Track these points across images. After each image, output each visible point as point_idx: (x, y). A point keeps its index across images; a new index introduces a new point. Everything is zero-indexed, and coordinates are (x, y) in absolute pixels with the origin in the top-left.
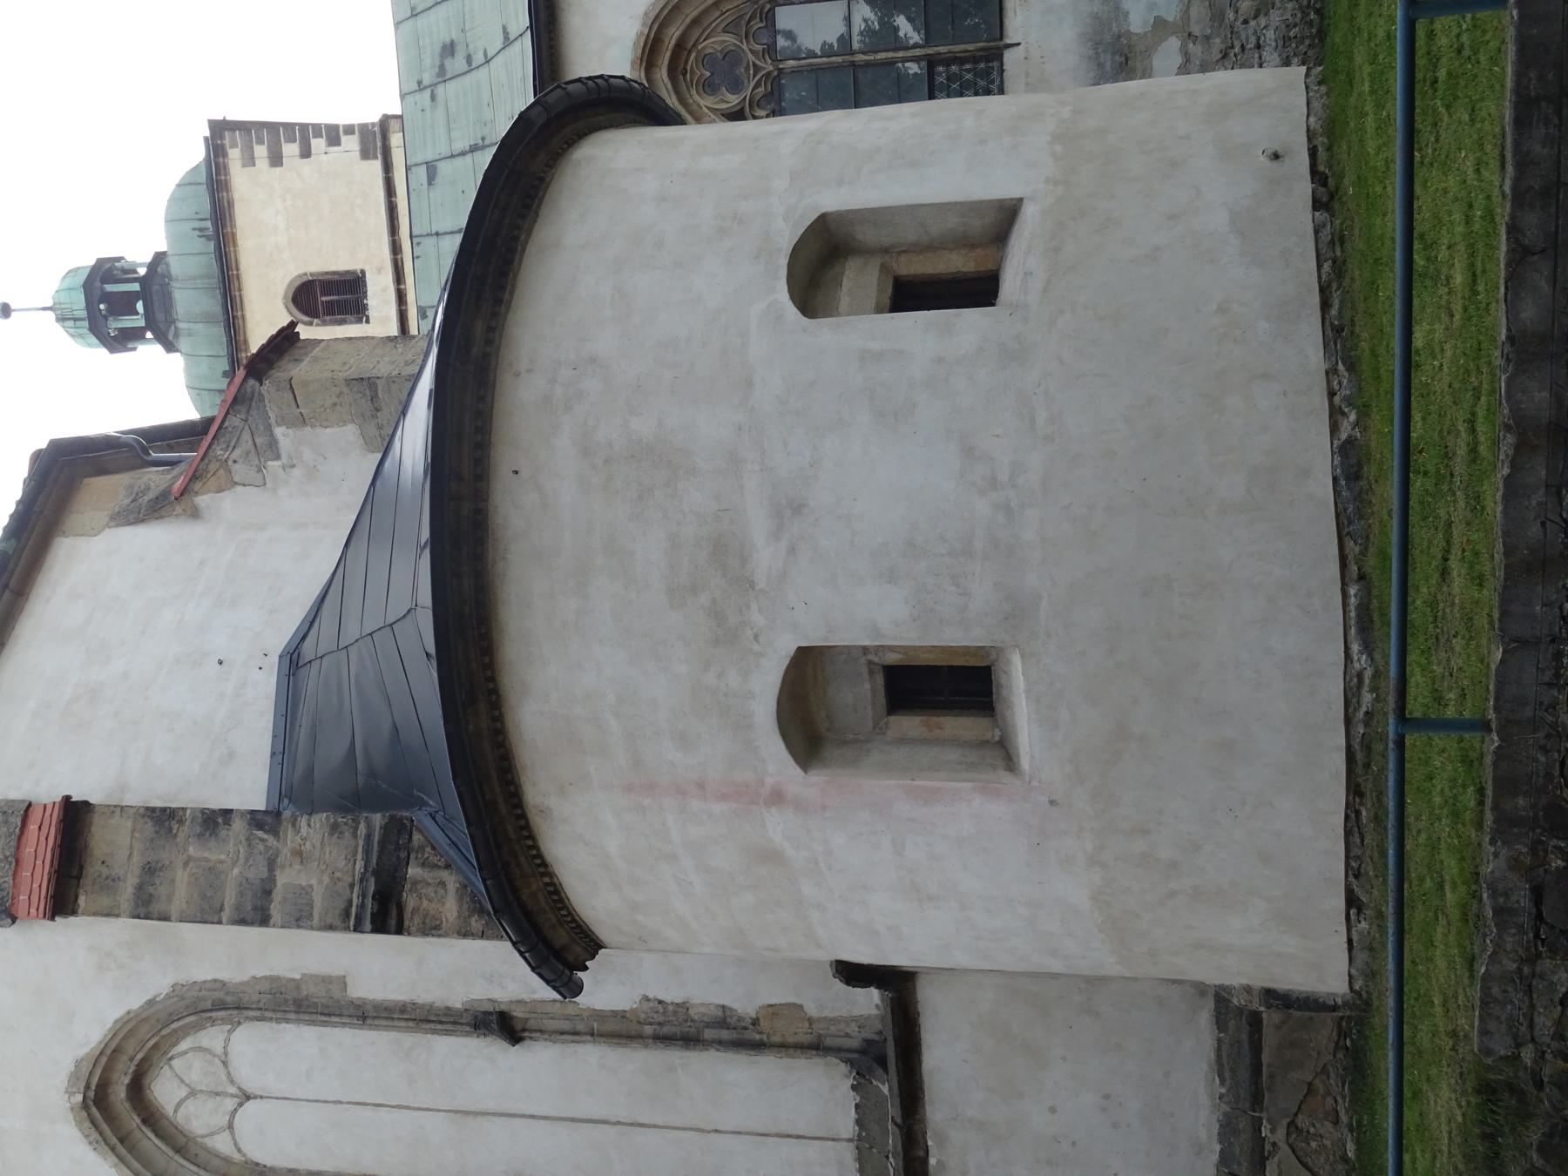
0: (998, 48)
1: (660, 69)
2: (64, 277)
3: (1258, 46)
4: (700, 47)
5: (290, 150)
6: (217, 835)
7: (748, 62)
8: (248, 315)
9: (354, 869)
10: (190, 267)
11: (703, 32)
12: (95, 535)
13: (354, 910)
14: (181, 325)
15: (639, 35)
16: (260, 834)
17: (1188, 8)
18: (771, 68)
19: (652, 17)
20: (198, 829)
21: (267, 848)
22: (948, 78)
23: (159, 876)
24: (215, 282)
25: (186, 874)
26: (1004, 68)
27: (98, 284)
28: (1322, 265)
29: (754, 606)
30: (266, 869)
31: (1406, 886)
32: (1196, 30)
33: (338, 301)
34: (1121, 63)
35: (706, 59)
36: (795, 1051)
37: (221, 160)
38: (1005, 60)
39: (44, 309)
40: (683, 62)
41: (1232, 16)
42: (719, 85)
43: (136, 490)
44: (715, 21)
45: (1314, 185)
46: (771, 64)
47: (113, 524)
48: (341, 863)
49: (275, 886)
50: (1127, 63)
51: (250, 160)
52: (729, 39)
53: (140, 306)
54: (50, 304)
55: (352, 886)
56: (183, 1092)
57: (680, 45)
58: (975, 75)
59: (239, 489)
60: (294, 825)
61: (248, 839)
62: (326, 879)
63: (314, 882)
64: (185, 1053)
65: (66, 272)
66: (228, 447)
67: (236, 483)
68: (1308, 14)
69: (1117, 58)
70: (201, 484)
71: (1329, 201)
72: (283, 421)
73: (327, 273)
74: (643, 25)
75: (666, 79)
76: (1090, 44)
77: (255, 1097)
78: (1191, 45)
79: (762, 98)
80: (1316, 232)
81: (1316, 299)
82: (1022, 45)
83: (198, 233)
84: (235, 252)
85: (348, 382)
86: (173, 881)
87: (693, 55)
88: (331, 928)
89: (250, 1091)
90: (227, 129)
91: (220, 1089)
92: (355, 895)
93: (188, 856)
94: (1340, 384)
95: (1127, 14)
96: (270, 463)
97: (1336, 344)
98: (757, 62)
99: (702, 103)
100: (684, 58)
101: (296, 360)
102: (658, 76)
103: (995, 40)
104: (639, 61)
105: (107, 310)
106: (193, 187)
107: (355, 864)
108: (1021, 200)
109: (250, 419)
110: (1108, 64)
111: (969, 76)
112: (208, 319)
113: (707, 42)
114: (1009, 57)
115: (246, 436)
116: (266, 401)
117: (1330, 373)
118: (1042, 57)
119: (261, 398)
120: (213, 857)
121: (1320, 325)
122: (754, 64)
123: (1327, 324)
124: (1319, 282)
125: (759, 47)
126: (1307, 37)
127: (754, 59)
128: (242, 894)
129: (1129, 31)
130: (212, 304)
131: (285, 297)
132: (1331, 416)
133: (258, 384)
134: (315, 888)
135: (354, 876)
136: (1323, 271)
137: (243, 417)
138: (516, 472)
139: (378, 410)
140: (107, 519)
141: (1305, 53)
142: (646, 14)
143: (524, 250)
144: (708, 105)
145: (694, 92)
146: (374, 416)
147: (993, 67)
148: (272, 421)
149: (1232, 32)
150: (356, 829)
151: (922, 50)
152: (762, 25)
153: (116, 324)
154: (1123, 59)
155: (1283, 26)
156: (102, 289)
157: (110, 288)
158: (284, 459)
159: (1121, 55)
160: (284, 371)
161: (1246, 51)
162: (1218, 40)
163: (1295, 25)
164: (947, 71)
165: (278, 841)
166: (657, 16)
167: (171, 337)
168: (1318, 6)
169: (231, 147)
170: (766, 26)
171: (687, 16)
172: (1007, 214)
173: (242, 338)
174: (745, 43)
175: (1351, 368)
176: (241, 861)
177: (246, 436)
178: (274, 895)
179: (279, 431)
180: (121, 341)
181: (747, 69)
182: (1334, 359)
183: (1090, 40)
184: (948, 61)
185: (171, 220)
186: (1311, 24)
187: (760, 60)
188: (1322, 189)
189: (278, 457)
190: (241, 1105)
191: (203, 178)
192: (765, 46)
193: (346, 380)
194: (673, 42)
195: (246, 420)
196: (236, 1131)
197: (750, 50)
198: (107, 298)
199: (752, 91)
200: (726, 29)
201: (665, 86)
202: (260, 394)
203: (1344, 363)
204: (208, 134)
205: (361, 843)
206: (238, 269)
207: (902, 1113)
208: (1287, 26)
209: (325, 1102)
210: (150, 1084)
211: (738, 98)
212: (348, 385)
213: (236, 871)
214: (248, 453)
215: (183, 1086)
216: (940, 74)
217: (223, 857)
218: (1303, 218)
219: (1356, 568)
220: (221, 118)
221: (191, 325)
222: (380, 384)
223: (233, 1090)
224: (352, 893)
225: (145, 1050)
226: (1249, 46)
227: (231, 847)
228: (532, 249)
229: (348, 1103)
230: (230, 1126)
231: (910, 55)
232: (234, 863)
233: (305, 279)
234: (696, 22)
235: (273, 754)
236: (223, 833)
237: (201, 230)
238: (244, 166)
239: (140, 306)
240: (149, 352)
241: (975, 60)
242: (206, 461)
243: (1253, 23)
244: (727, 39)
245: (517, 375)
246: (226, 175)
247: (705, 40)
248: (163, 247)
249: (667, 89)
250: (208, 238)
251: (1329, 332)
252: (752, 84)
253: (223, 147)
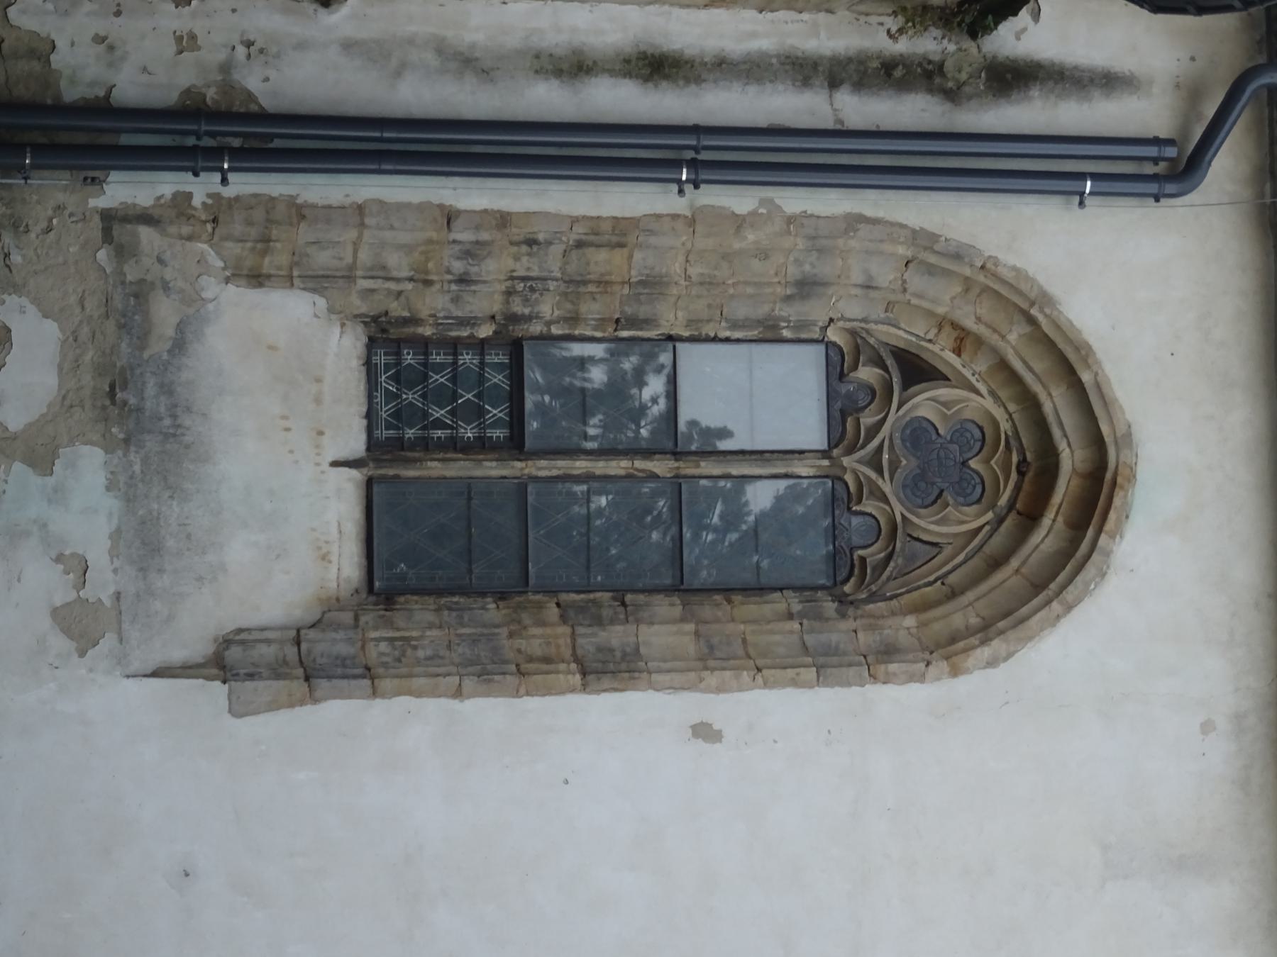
0: (379, 462)
1: (1074, 469)
4: (990, 515)
15: (1117, 533)
18: (846, 461)
22: (481, 412)
26: (365, 422)
34: (124, 387)
35: (980, 494)
36: (707, 334)
40: (1026, 486)
42: (951, 441)
44: (960, 565)
46: (844, 469)
50: (112, 387)
52: (928, 525)
57: (1031, 518)
58: (426, 415)
74: (1108, 554)
75: (1062, 446)
79: (866, 407)
82: (331, 459)
87: (1003, 501)
98: (873, 475)
99: (988, 403)
100: (1022, 495)
102: (1080, 454)
103: (383, 479)
104: (1119, 480)
110: (151, 389)
111: (438, 413)
114: (356, 444)
118: (288, 430)
122: (880, 471)
127: (880, 482)
129: (106, 453)
144: (979, 399)
145: (1005, 426)
151: (535, 472)
152: (861, 552)
159: (125, 403)
164: (482, 427)
170: (852, 550)
171: (1017, 571)
174: (899, 518)
181: (894, 466)
183: (187, 447)
184: (482, 446)
187: (868, 478)
194: (1046, 521)
197: (887, 501)
199: (884, 419)
200: (935, 550)
207: (493, 696)
211: (915, 407)
216: (499, 367)
234: (996, 563)
241: (426, 446)
244: (933, 527)
247: (983, 526)
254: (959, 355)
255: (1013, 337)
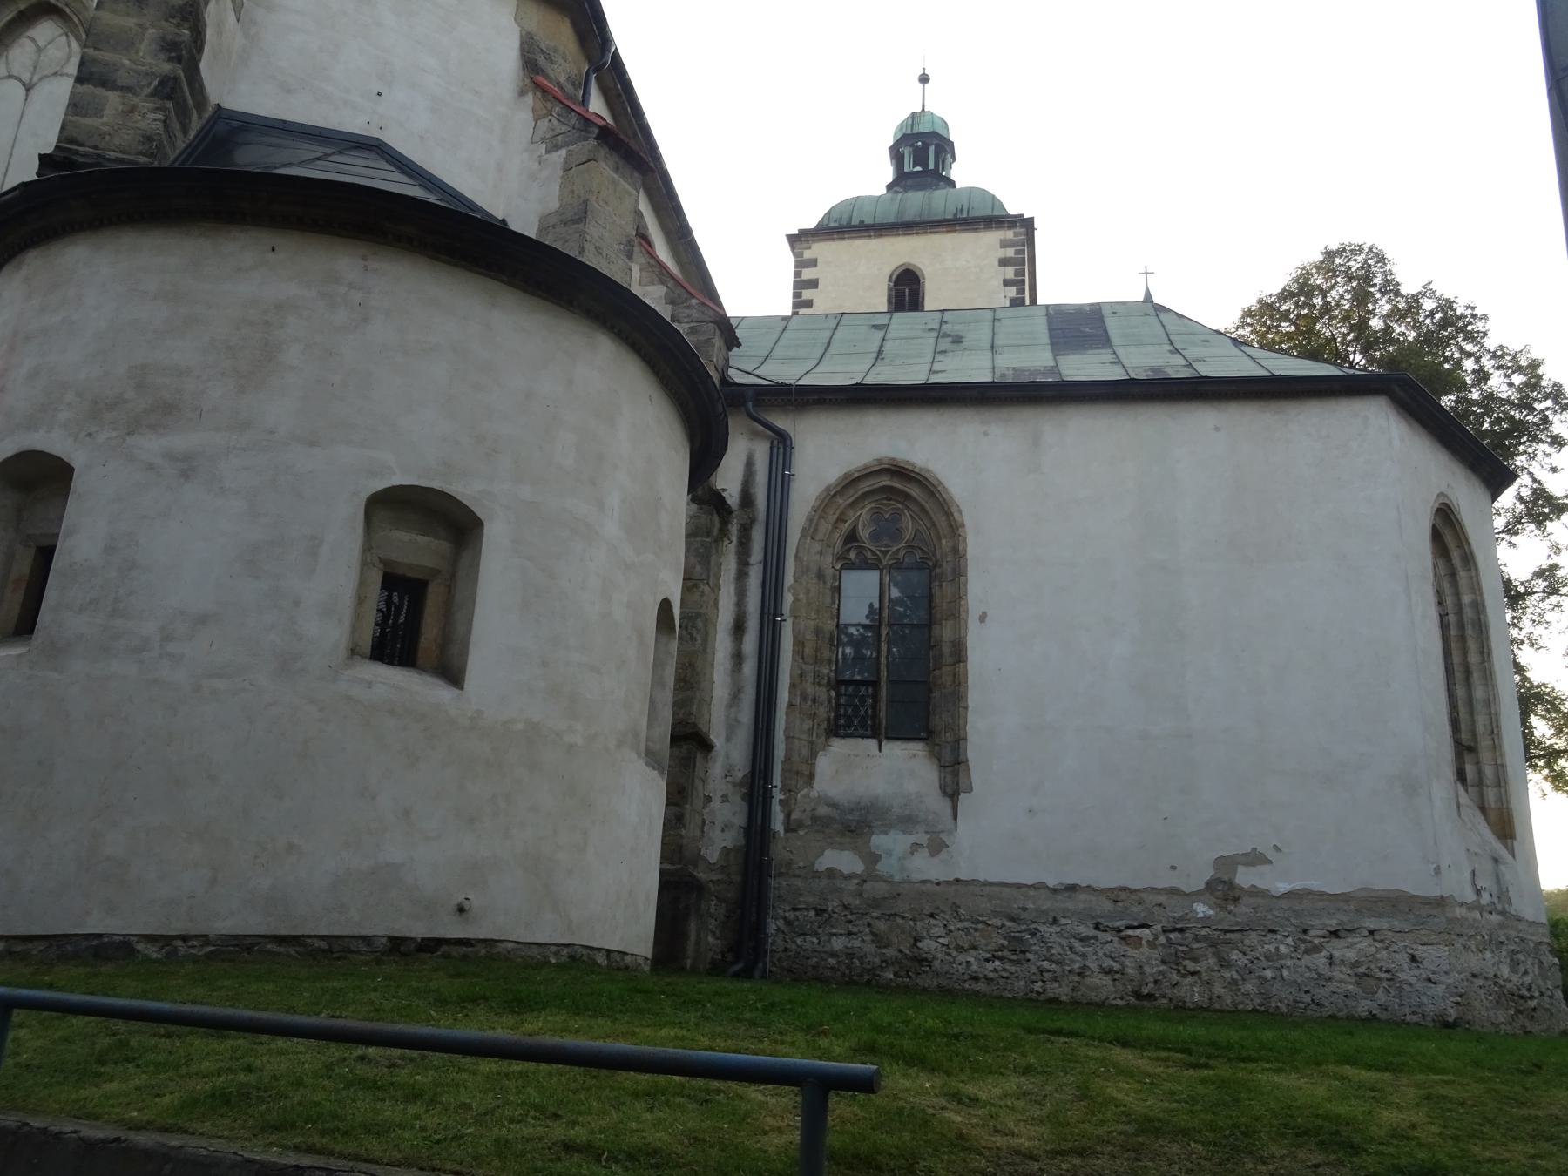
2: (942, 120)
3: (850, 933)
4: (906, 511)
5: (1010, 273)
6: (160, 51)
7: (889, 546)
8: (900, 238)
9: (109, 150)
10: (937, 202)
11: (917, 515)
12: (515, 19)
13: (75, 147)
14: (900, 195)
15: (913, 465)
16: (156, 83)
17: (885, 881)
19: (927, 475)
20: (169, 37)
21: (142, 87)
23: (134, 5)
24: (926, 218)
25: (133, 25)
27: (935, 141)
28: (324, 940)
29: (114, 434)
30: (124, 84)
31: (54, 1014)
32: (867, 886)
33: (905, 300)
37: (1006, 225)
38: (870, 740)
39: (923, 106)
41: (875, 914)
43: (553, 54)
45: (419, 940)
47: (524, 33)
48: (117, 141)
49: (107, 91)
50: (849, 831)
51: (1004, 244)
52: (908, 534)
53: (918, 169)
54: (926, 110)
55: (96, 147)
56: (41, 43)
57: (907, 496)
59: (533, 123)
60: (157, 109)
61: (153, 73)
62: (105, 129)
63: (105, 119)
64: (69, 46)
65: (946, 120)
66: (559, 115)
67: (536, 122)
68: (869, 975)
69: (855, 824)
70: (540, 96)
71: (400, 952)
72: (569, 154)
73: (924, 294)
74: (921, 469)
75: (881, 484)
76: (869, 804)
77: (27, 95)
78: (856, 881)
80: (363, 938)
81: (284, 931)
83: (960, 207)
84: (943, 232)
85: (586, 202)
86: (128, 15)
88: (63, 128)
89: (32, 91)
90: (1027, 230)
91: (38, 70)
92: (87, 149)
93: (147, 29)
94: (193, 947)
95: (886, 833)
96: (544, 146)
97: (237, 945)
98: (890, 553)
99: (864, 511)
101: (618, 168)
103: (886, 733)
105: (917, 146)
106: (991, 206)
107: (114, 151)
108: (461, 688)
109: (574, 131)
111: (862, 712)
112: (900, 213)
113: (909, 518)
114: (873, 743)
115: (564, 128)
116: (583, 143)
117: (205, 939)
119: (586, 139)
120: (143, 47)
121: (257, 933)
122: (888, 551)
123: (260, 940)
124: (303, 936)
125: (901, 556)
126: (851, 972)
128: (106, 64)
130: (909, 216)
131: (910, 264)
132: (162, 936)
133: (594, 136)
134: (100, 120)
135: (103, 149)
136: (316, 940)
137: (576, 126)
138: (273, 250)
139: (565, 224)
140: (530, 30)
141: (839, 970)
142: (928, 471)
143: (491, 277)
145: (873, 505)
146: (561, 221)
147: (867, 730)
148: (571, 148)
149: (862, 914)
150: (144, 154)
153: (907, 152)
154: (853, 828)
155: (862, 954)
156: (932, 144)
157: (932, 149)
158: (545, 157)
159: (855, 827)
160: (605, 157)
161: (847, 924)
162: (857, 902)
163: (861, 964)
165: (146, 96)
166: (926, 479)
167: (895, 188)
168: (874, 982)
169: (1014, 233)
170: (916, 561)
172: (452, 675)
173: (884, 233)
175: (209, 956)
176: (134, 67)
177: (564, 128)
178: (100, 89)
179: (563, 152)
180: (896, 153)
181: (886, 546)
182: (218, 942)
184: (875, 696)
185: (971, 190)
186: (861, 976)
188: (412, 946)
189: (548, 152)
190: (24, 85)
191: (996, 213)
192: (901, 560)
193: (588, 200)
194: (909, 491)
195: (574, 128)
196: (6, 81)
197: (899, 549)
198: (926, 148)
201: (874, 484)
202: (589, 138)
203: (212, 952)
204: (1025, 216)
205: (131, 158)
206: (931, 233)
208: (862, 957)
209: (13, 147)
210: (52, 20)
212: (584, 202)
213: (126, 62)
214: (553, 130)
215: (46, 43)
217: (141, 54)
218: (380, 926)
219: (18, 950)
220: (1036, 227)
221: (898, 201)
222: (580, 226)
223: (35, 79)
224: (89, 147)
225: (71, 14)
226: (850, 927)
227: (149, 60)
228: (492, 284)
229: (9, 163)
230: (10, 77)
231: (882, 668)
232: (134, 62)
233: (919, 274)
234: (923, 509)
235: (285, 122)
236: (162, 56)
237: (961, 210)
238: (1001, 240)
239: (918, 169)
240: (887, 173)
242: (553, 99)
243: (867, 930)
245: (364, 258)
246: (996, 228)
247: (911, 515)
248: (958, 186)
249: (874, 484)
250: (956, 215)
251: (249, 941)
252: (874, 549)
253: (1015, 226)
254: (846, 521)
255: (841, 501)
